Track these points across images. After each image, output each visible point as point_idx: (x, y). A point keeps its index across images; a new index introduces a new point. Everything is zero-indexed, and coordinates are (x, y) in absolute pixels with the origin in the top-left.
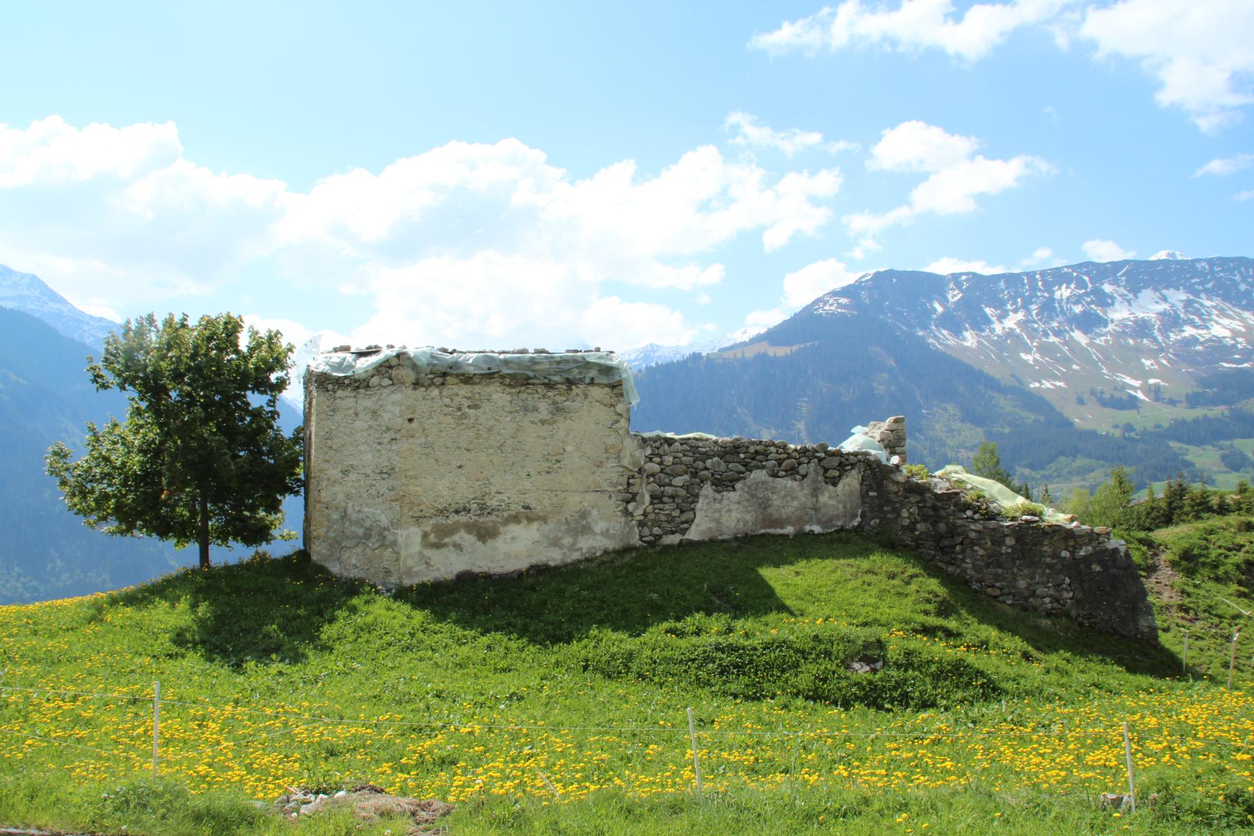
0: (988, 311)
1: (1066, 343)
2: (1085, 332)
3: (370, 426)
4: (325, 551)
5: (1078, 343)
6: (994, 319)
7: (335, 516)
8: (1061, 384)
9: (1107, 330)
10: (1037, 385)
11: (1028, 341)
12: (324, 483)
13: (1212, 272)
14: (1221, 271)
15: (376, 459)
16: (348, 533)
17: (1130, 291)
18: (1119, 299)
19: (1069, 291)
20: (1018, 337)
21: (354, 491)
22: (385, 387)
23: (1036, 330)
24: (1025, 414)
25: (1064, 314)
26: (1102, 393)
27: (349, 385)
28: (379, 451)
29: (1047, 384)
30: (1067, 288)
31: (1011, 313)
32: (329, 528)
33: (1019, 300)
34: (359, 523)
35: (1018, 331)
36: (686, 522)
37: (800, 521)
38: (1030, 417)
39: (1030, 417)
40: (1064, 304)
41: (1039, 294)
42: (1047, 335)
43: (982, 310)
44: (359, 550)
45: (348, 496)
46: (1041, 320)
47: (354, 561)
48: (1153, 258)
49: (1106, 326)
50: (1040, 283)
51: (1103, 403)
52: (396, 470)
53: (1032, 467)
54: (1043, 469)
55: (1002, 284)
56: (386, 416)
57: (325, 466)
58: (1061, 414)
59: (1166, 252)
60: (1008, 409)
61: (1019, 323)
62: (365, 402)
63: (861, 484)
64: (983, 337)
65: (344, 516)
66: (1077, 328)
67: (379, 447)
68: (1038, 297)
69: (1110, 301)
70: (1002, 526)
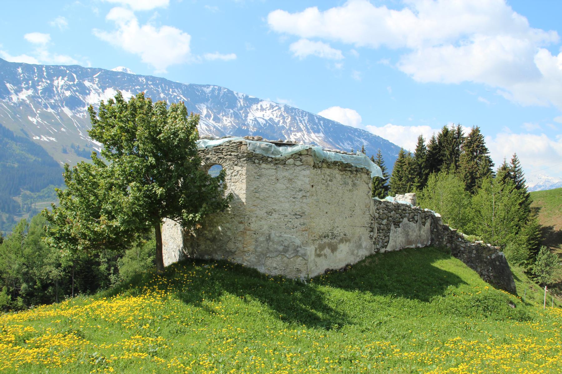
0: (8, 85)
1: (58, 114)
2: (71, 109)
3: (287, 188)
4: (254, 260)
5: (67, 115)
6: (13, 92)
7: (262, 239)
8: (54, 139)
9: (85, 109)
10: (38, 138)
11: (34, 109)
12: (254, 219)
13: (147, 84)
14: (152, 84)
15: (292, 207)
16: (271, 249)
17: (100, 88)
18: (93, 91)
19: (63, 81)
20: (28, 106)
21: (276, 224)
22: (298, 166)
23: (39, 102)
24: (30, 156)
25: (59, 96)
26: (79, 147)
27: (271, 162)
28: (294, 202)
29: (44, 138)
30: (62, 79)
31: (24, 90)
32: (256, 246)
33: (30, 82)
34: (281, 243)
35: (28, 102)
36: (386, 242)
37: (417, 242)
38: (32, 158)
39: (32, 158)
40: (59, 89)
41: (44, 80)
42: (46, 107)
43: (4, 84)
44: (278, 259)
45: (271, 227)
46: (43, 97)
47: (275, 265)
48: (114, 70)
49: (84, 107)
50: (45, 74)
51: (79, 154)
52: (306, 214)
53: (32, 190)
54: (39, 191)
55: (20, 70)
56: (299, 183)
57: (254, 209)
58: (52, 158)
59: (122, 68)
60: (18, 151)
61: (29, 97)
62: (283, 173)
63: (430, 226)
64: (4, 102)
65: (269, 239)
66: (67, 105)
67: (294, 200)
68: (43, 82)
69: (88, 91)
70: (472, 245)
